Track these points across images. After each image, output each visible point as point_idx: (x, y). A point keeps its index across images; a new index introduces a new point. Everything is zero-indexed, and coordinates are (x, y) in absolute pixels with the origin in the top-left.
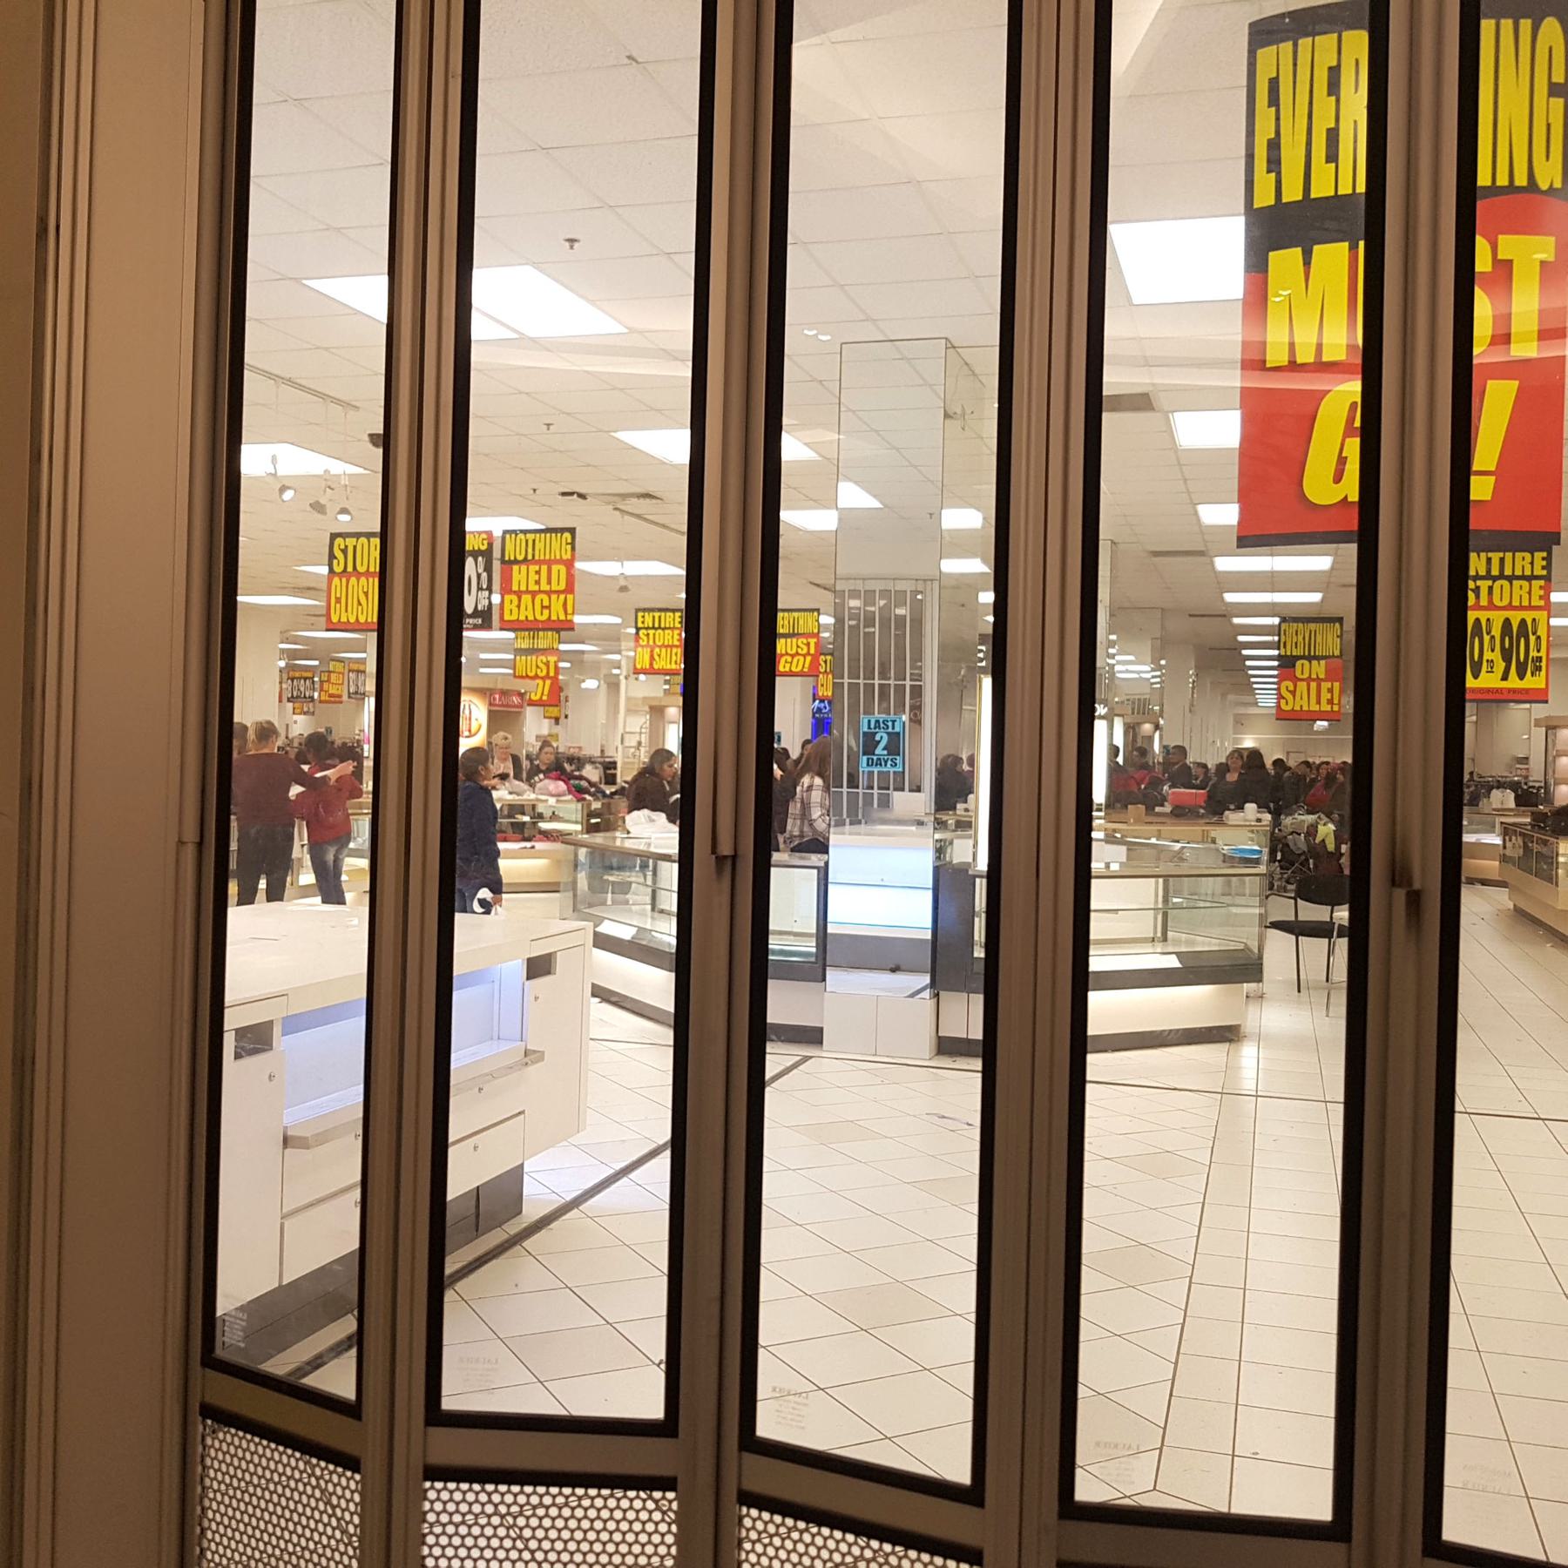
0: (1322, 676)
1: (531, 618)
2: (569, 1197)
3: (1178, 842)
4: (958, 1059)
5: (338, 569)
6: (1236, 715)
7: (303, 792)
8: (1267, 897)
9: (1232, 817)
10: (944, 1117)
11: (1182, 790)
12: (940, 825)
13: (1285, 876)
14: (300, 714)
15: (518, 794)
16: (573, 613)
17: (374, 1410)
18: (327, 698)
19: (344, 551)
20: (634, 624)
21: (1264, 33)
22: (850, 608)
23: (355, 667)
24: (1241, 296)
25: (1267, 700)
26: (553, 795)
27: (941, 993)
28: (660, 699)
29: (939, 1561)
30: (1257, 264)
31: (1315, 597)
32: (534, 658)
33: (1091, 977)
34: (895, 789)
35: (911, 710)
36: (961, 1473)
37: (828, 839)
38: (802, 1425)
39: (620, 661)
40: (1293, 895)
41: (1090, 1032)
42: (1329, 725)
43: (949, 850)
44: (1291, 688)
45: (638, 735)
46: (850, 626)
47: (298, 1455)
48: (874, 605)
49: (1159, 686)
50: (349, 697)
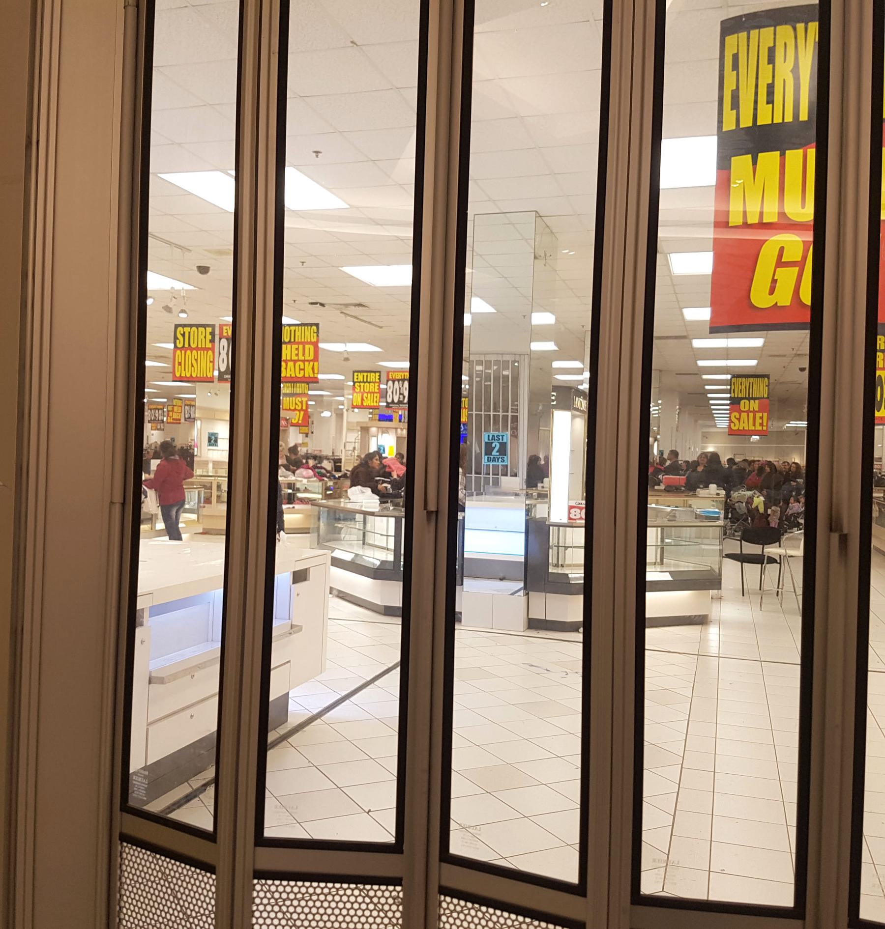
0: (756, 409)
1: (293, 375)
2: (315, 712)
3: (669, 506)
4: (540, 631)
5: (180, 345)
6: (703, 432)
7: (557, 350)
8: (724, 539)
9: (701, 492)
10: (532, 666)
11: (671, 476)
12: (528, 496)
13: (734, 527)
14: (155, 430)
15: (285, 477)
16: (318, 373)
17: (224, 836)
18: (171, 421)
19: (183, 335)
20: (352, 380)
21: (730, 27)
22: (476, 371)
23: (188, 403)
24: (713, 182)
25: (722, 424)
26: (305, 478)
27: (530, 592)
28: (367, 423)
29: (543, 925)
30: (724, 165)
31: (753, 363)
32: (294, 398)
33: (647, 584)
34: (502, 475)
35: (511, 430)
36: (572, 876)
37: (465, 504)
38: (477, 847)
39: (343, 401)
40: (739, 539)
41: (647, 616)
42: (760, 438)
43: (533, 510)
44: (738, 416)
45: (353, 443)
46: (477, 382)
47: (148, 853)
48: (490, 369)
49: (657, 415)
50: (185, 420)
